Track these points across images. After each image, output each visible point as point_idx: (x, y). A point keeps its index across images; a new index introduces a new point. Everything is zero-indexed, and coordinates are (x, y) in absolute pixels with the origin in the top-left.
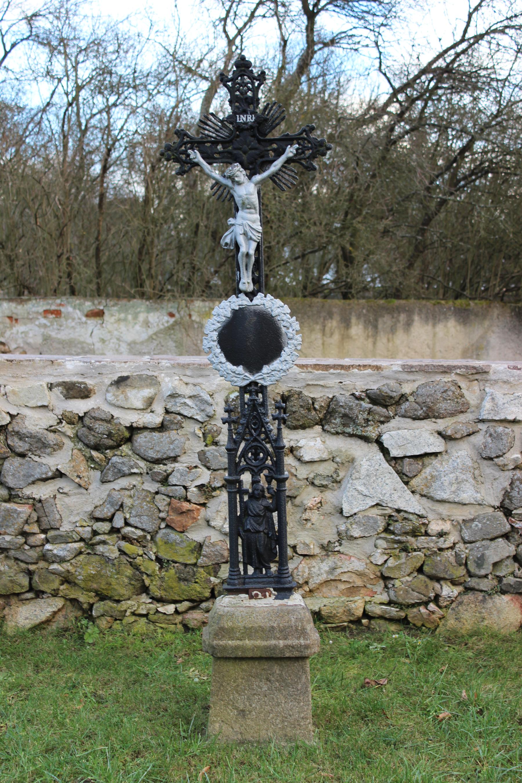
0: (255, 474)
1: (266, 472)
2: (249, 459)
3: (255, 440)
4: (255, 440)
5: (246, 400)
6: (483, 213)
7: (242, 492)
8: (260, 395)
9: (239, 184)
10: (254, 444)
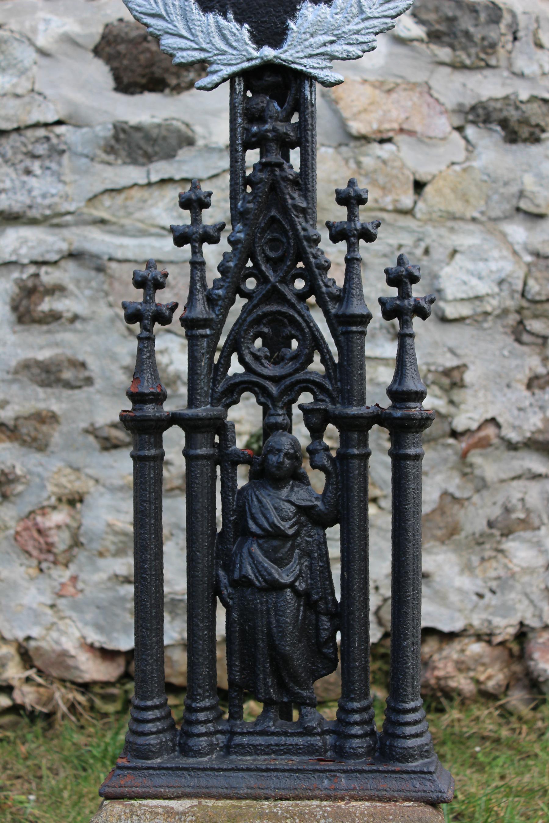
2: (256, 358)
3: (274, 295)
8: (295, 156)
10: (267, 308)
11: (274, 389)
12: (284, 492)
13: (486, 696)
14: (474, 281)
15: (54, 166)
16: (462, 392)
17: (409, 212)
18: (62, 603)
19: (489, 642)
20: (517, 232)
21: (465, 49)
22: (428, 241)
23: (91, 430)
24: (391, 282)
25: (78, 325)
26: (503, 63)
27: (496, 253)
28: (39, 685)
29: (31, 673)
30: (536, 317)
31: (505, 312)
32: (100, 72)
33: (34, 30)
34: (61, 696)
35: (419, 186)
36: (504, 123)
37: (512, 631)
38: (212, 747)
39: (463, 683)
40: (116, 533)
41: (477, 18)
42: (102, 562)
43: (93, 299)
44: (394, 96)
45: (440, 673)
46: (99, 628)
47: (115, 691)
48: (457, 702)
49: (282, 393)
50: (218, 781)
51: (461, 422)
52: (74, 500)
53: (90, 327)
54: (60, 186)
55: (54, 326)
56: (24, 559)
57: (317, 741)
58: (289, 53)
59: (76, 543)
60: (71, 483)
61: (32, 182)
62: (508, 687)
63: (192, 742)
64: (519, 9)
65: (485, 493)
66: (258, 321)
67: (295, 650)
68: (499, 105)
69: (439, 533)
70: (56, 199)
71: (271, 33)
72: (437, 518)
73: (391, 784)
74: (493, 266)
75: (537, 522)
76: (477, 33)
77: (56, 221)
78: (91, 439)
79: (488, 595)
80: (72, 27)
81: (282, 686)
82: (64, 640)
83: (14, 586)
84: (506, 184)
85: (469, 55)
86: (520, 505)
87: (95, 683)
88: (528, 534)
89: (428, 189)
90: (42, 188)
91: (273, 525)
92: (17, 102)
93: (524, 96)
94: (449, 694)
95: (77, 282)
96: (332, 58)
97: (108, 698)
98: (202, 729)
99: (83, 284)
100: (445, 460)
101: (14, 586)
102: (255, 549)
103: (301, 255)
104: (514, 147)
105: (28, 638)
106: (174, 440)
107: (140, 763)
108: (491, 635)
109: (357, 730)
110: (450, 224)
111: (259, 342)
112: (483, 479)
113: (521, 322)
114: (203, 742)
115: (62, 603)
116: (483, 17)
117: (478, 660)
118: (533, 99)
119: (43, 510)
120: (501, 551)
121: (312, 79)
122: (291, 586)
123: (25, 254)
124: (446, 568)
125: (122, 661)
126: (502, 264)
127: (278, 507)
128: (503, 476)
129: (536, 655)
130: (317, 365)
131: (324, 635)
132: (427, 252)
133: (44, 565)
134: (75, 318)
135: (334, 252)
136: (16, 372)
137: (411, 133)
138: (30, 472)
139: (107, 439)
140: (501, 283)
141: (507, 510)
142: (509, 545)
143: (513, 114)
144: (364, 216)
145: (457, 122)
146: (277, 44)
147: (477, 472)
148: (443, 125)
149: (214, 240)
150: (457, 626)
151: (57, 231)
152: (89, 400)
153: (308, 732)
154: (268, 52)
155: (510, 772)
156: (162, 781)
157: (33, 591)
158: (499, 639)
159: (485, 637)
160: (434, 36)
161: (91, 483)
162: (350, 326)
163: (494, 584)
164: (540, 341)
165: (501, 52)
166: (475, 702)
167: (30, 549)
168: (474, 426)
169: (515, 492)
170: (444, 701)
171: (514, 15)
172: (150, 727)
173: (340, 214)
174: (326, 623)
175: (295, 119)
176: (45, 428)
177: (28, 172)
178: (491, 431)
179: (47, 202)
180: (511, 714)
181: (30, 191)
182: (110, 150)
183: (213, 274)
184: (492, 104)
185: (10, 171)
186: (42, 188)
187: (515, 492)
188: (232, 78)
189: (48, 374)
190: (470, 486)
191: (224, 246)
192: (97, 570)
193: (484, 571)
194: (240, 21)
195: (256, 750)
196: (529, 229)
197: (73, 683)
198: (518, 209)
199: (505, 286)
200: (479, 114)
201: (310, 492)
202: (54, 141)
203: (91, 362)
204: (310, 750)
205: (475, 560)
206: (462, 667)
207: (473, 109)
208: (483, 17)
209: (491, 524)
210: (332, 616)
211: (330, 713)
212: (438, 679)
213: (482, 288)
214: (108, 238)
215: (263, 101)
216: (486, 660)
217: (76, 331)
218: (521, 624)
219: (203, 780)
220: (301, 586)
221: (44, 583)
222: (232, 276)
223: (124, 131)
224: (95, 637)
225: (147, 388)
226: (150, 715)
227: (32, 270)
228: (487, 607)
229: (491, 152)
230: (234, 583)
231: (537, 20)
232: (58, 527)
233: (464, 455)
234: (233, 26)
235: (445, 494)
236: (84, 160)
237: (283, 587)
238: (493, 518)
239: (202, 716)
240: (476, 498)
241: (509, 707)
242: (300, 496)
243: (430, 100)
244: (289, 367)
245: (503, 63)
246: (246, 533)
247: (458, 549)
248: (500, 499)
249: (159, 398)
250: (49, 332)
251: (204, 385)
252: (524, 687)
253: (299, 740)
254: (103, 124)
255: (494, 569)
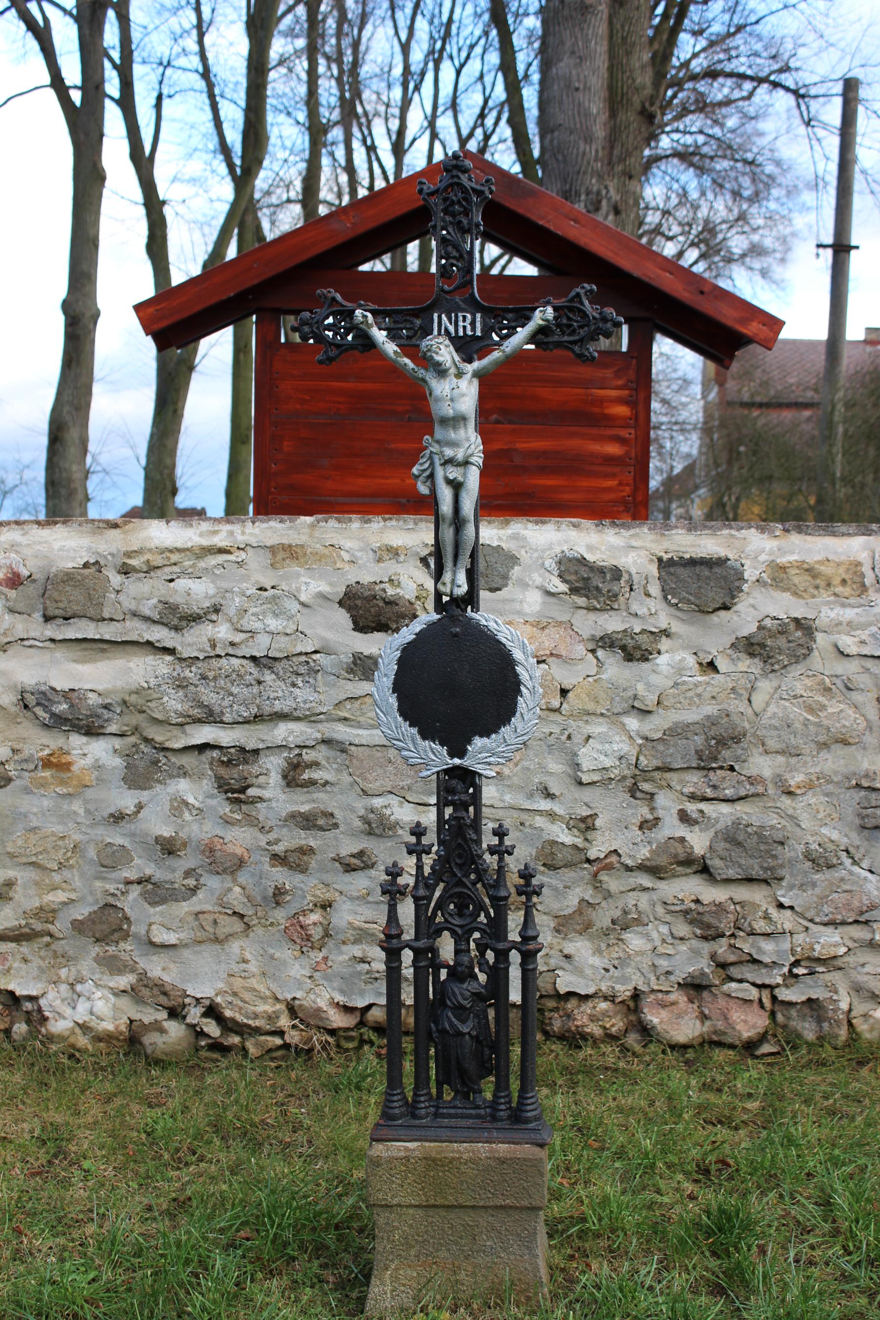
0: (461, 940)
1: (477, 935)
2: (451, 915)
3: (460, 883)
4: (460, 883)
5: (447, 817)
6: (173, 1084)
7: (437, 965)
8: (471, 809)
9: (441, 372)
10: (457, 890)
11: (459, 931)
12: (465, 985)
13: (611, 1037)
14: (602, 758)
15: (311, 680)
16: (593, 833)
17: (557, 711)
18: (317, 975)
19: (613, 1001)
20: (633, 723)
21: (596, 598)
22: (570, 730)
23: (337, 859)
24: (521, 876)
25: (328, 788)
26: (623, 607)
27: (617, 738)
28: (302, 1030)
29: (296, 1021)
30: (646, 781)
31: (624, 778)
32: (343, 618)
33: (298, 590)
34: (318, 1038)
35: (564, 692)
36: (623, 648)
37: (628, 994)
38: (427, 1115)
39: (594, 1029)
40: (355, 929)
41: (604, 577)
42: (344, 948)
43: (338, 771)
44: (547, 631)
45: (579, 1023)
46: (342, 992)
47: (353, 1034)
48: (590, 1042)
49: (464, 934)
50: (431, 1133)
51: (593, 854)
52: (326, 906)
53: (336, 789)
54: (316, 695)
55: (311, 789)
56: (290, 945)
57: (482, 1112)
58: (466, 762)
59: (327, 934)
60: (323, 894)
61: (297, 691)
62: (626, 1031)
63: (417, 1112)
64: (633, 571)
65: (610, 900)
66: (451, 896)
67: (471, 1066)
68: (620, 636)
69: (578, 927)
70: (314, 704)
71: (458, 751)
72: (577, 917)
73: (519, 1135)
74: (616, 747)
75: (646, 920)
76: (604, 587)
77: (313, 719)
78: (337, 864)
79: (612, 969)
80: (323, 587)
81: (464, 1083)
82: (318, 1000)
83: (284, 963)
84: (624, 690)
85: (599, 603)
86: (634, 909)
87: (340, 1029)
88: (640, 929)
89: (570, 694)
90: (303, 696)
91: (459, 1002)
92: (287, 638)
93: (637, 630)
94: (584, 1037)
95: (328, 759)
96: (489, 764)
97: (350, 1039)
98: (423, 1105)
99: (332, 760)
100: (582, 878)
101: (284, 963)
102: (450, 1014)
103: (474, 862)
104: (630, 664)
105: (294, 999)
106: (407, 956)
107: (391, 1123)
108: (614, 997)
109: (503, 1107)
110: (585, 718)
111: (452, 906)
112: (609, 891)
113: (635, 784)
114: (423, 1111)
115: (317, 975)
116: (608, 577)
117: (605, 1014)
118: (643, 631)
119: (304, 913)
120: (621, 940)
121: (480, 775)
122: (469, 1033)
123: (292, 741)
124: (583, 951)
125: (358, 1014)
126: (621, 745)
127: (462, 992)
128: (623, 889)
129: (645, 1010)
130: (482, 918)
131: (486, 1057)
132: (569, 737)
133: (305, 949)
134: (327, 783)
135: (491, 860)
136: (286, 821)
137: (558, 656)
138: (295, 888)
139: (348, 865)
140: (621, 758)
141: (625, 912)
142: (626, 936)
143: (630, 643)
144: (508, 841)
145: (591, 646)
146: (461, 757)
147: (604, 886)
148: (580, 650)
149: (428, 853)
150: (591, 991)
151: (313, 725)
152: (336, 838)
153: (478, 1107)
154: (457, 761)
155: (619, 1096)
156: (402, 1132)
157: (297, 966)
158: (620, 999)
159: (610, 998)
160: (574, 591)
161: (337, 894)
162: (501, 904)
163: (616, 962)
164: (648, 797)
165: (621, 599)
166: (603, 1042)
167: (295, 938)
168: (602, 856)
169: (631, 900)
170: (581, 1043)
171: (630, 575)
172: (395, 1104)
173: (495, 841)
174: (487, 1052)
175: (471, 790)
176: (305, 858)
177: (294, 685)
178: (614, 859)
179: (307, 706)
180: (628, 1050)
181: (295, 698)
182: (350, 671)
183: (427, 870)
184: (615, 635)
185: (282, 684)
186: (303, 696)
187: (631, 900)
188: (438, 773)
189: (305, 821)
190: (600, 895)
191: (433, 856)
192: (341, 953)
193: (610, 954)
194: (442, 745)
195: (450, 1116)
196: (640, 721)
197: (325, 1029)
198: (633, 707)
199: (623, 761)
200: (606, 642)
201: (479, 984)
202: (312, 664)
203: (336, 812)
204: (478, 1116)
205: (603, 946)
206: (593, 1018)
207: (602, 638)
208: (608, 577)
209: (613, 922)
210: (490, 1048)
211: (489, 1096)
212: (577, 1026)
213: (608, 763)
214: (348, 730)
215: (454, 782)
216: (611, 1014)
217: (327, 792)
218: (635, 989)
219: (423, 1133)
220: (474, 1033)
221: (304, 961)
222: (437, 874)
223: (360, 659)
224: (339, 998)
225: (394, 932)
226: (395, 1098)
227: (297, 751)
228: (612, 977)
229: (614, 668)
230: (438, 1031)
231: (646, 578)
232: (315, 924)
233: (595, 875)
234: (439, 747)
235: (583, 900)
236: (333, 677)
237: (464, 1034)
238: (615, 917)
239: (422, 1099)
240: (604, 904)
241: (626, 1045)
242: (472, 986)
243: (572, 633)
244: (468, 920)
245: (623, 607)
246: (445, 1005)
247: (591, 938)
248: (621, 905)
249: (399, 936)
250: (308, 792)
251: (423, 930)
252: (638, 1031)
253: (473, 1112)
254: (346, 653)
255: (616, 952)
